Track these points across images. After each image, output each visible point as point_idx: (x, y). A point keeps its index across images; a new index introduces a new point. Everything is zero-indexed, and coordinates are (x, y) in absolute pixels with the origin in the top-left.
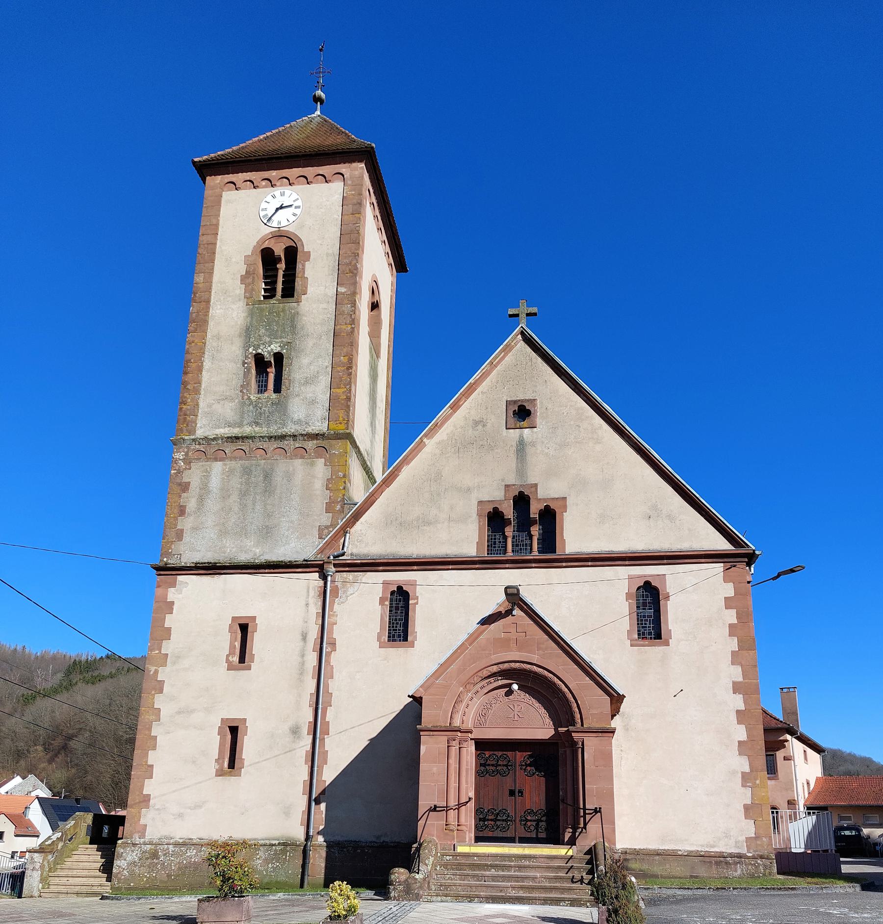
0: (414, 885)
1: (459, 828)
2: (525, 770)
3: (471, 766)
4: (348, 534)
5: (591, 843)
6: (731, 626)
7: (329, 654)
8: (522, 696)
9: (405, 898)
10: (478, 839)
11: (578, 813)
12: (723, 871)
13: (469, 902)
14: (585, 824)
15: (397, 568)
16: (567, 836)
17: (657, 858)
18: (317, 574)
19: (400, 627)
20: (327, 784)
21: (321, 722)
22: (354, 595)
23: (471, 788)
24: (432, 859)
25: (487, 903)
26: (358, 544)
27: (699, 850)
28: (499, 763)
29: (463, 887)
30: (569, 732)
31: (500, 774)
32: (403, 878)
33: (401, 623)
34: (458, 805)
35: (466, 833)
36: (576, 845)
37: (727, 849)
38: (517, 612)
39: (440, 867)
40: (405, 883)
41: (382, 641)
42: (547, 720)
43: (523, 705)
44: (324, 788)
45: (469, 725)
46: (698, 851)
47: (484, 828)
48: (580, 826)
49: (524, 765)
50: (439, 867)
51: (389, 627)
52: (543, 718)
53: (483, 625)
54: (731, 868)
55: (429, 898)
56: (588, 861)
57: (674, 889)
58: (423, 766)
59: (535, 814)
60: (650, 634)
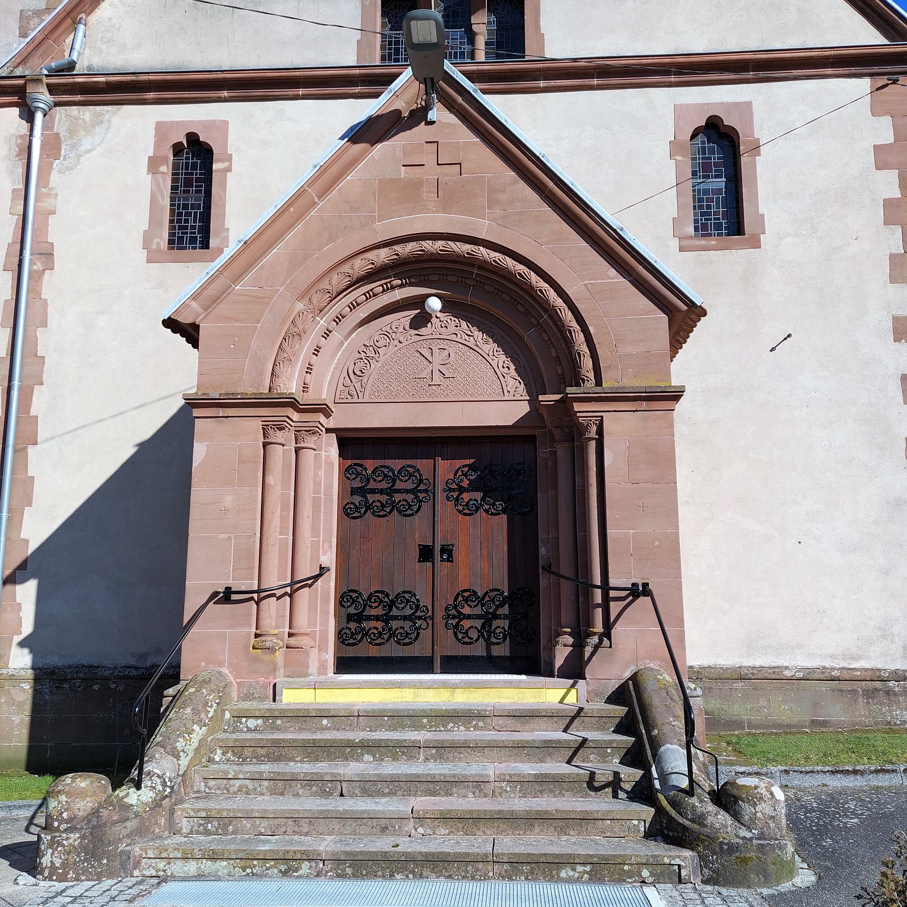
0: (118, 828)
1: (293, 641)
2: (457, 500)
3: (328, 494)
4: (82, 27)
5: (624, 672)
6: (888, 204)
7: (36, 277)
8: (452, 328)
9: (85, 871)
10: (344, 665)
11: (588, 596)
12: (881, 710)
13: (285, 873)
14: (608, 626)
15: (187, 94)
16: (561, 655)
17: (740, 685)
18: (16, 111)
19: (195, 222)
20: (31, 550)
21: (18, 418)
22: (93, 152)
23: (326, 545)
24: (199, 732)
25: (338, 876)
26: (104, 46)
27: (827, 666)
28: (396, 487)
29: (272, 822)
30: (565, 403)
31: (400, 512)
32: (83, 806)
33: (196, 213)
34: (291, 585)
35: (307, 653)
36: (585, 679)
37: (886, 662)
38: (437, 113)
39: (224, 754)
40: (89, 821)
41: (154, 247)
42: (511, 382)
43: (452, 348)
44: (23, 557)
45: (323, 393)
46: (824, 668)
47: (359, 637)
48: (595, 630)
49: (454, 490)
50: (219, 752)
51: (171, 221)
52: (501, 377)
53: (355, 143)
54: (898, 703)
55: (162, 865)
56: (620, 723)
57: (821, 776)
58: (199, 493)
59: (481, 601)
60: (718, 227)
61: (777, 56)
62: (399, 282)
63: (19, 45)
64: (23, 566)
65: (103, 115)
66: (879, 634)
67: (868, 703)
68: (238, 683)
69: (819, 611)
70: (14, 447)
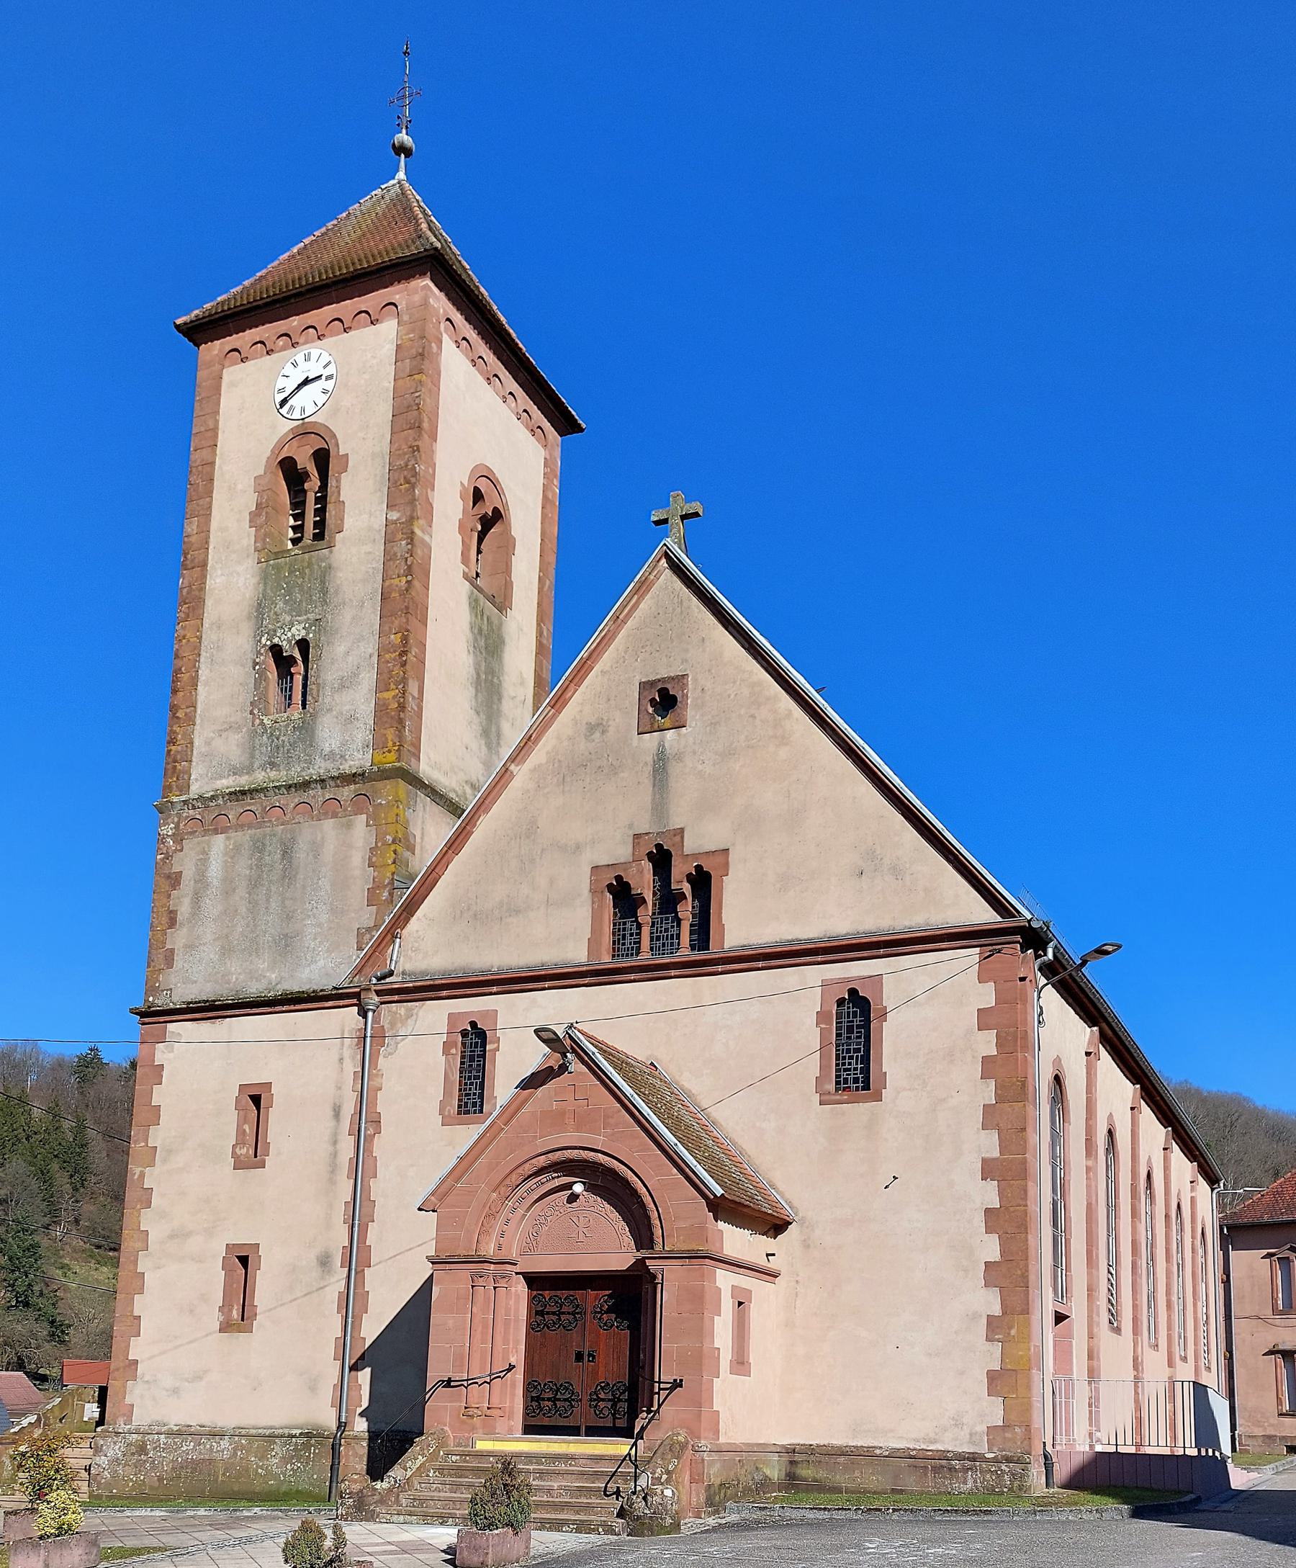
0: (370, 1498)
7: (369, 1139)
10: (529, 1429)
13: (441, 1524)
17: (842, 1459)
24: (421, 1460)
33: (476, 1082)
50: (432, 1471)
52: (620, 1236)
61: (898, 937)
62: (556, 1175)
63: (356, 958)
64: (362, 1357)
65: (413, 1009)
66: (953, 1423)
67: (935, 1477)
68: (454, 1436)
69: (908, 1403)
70: (356, 1270)
